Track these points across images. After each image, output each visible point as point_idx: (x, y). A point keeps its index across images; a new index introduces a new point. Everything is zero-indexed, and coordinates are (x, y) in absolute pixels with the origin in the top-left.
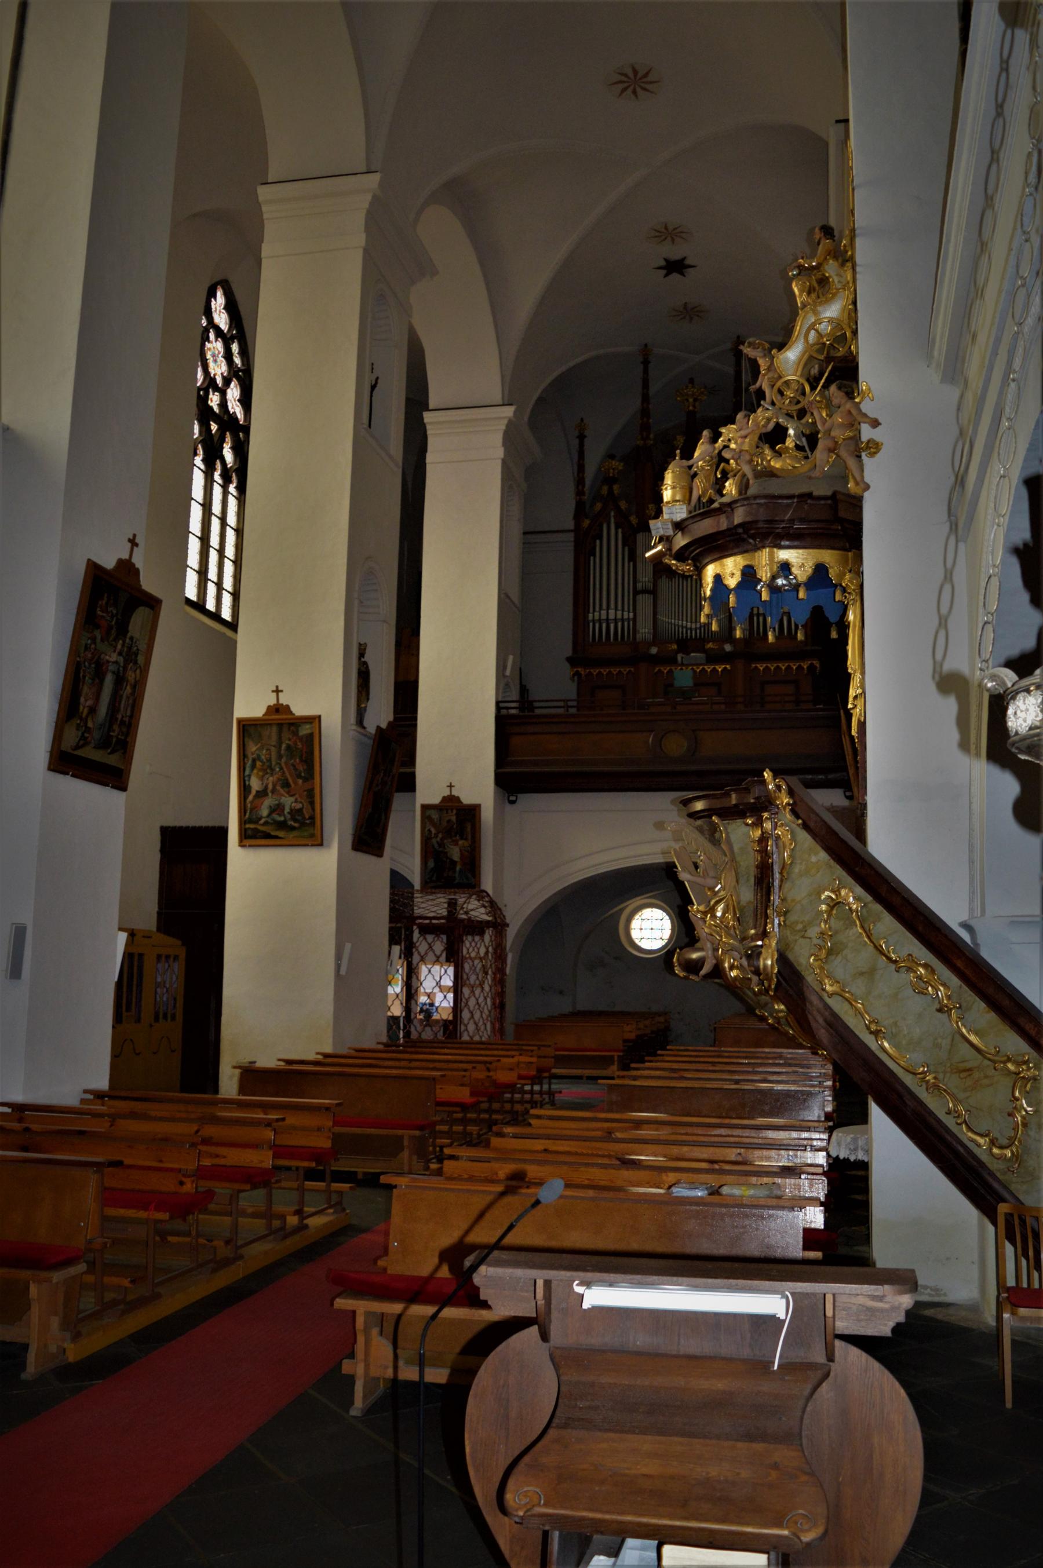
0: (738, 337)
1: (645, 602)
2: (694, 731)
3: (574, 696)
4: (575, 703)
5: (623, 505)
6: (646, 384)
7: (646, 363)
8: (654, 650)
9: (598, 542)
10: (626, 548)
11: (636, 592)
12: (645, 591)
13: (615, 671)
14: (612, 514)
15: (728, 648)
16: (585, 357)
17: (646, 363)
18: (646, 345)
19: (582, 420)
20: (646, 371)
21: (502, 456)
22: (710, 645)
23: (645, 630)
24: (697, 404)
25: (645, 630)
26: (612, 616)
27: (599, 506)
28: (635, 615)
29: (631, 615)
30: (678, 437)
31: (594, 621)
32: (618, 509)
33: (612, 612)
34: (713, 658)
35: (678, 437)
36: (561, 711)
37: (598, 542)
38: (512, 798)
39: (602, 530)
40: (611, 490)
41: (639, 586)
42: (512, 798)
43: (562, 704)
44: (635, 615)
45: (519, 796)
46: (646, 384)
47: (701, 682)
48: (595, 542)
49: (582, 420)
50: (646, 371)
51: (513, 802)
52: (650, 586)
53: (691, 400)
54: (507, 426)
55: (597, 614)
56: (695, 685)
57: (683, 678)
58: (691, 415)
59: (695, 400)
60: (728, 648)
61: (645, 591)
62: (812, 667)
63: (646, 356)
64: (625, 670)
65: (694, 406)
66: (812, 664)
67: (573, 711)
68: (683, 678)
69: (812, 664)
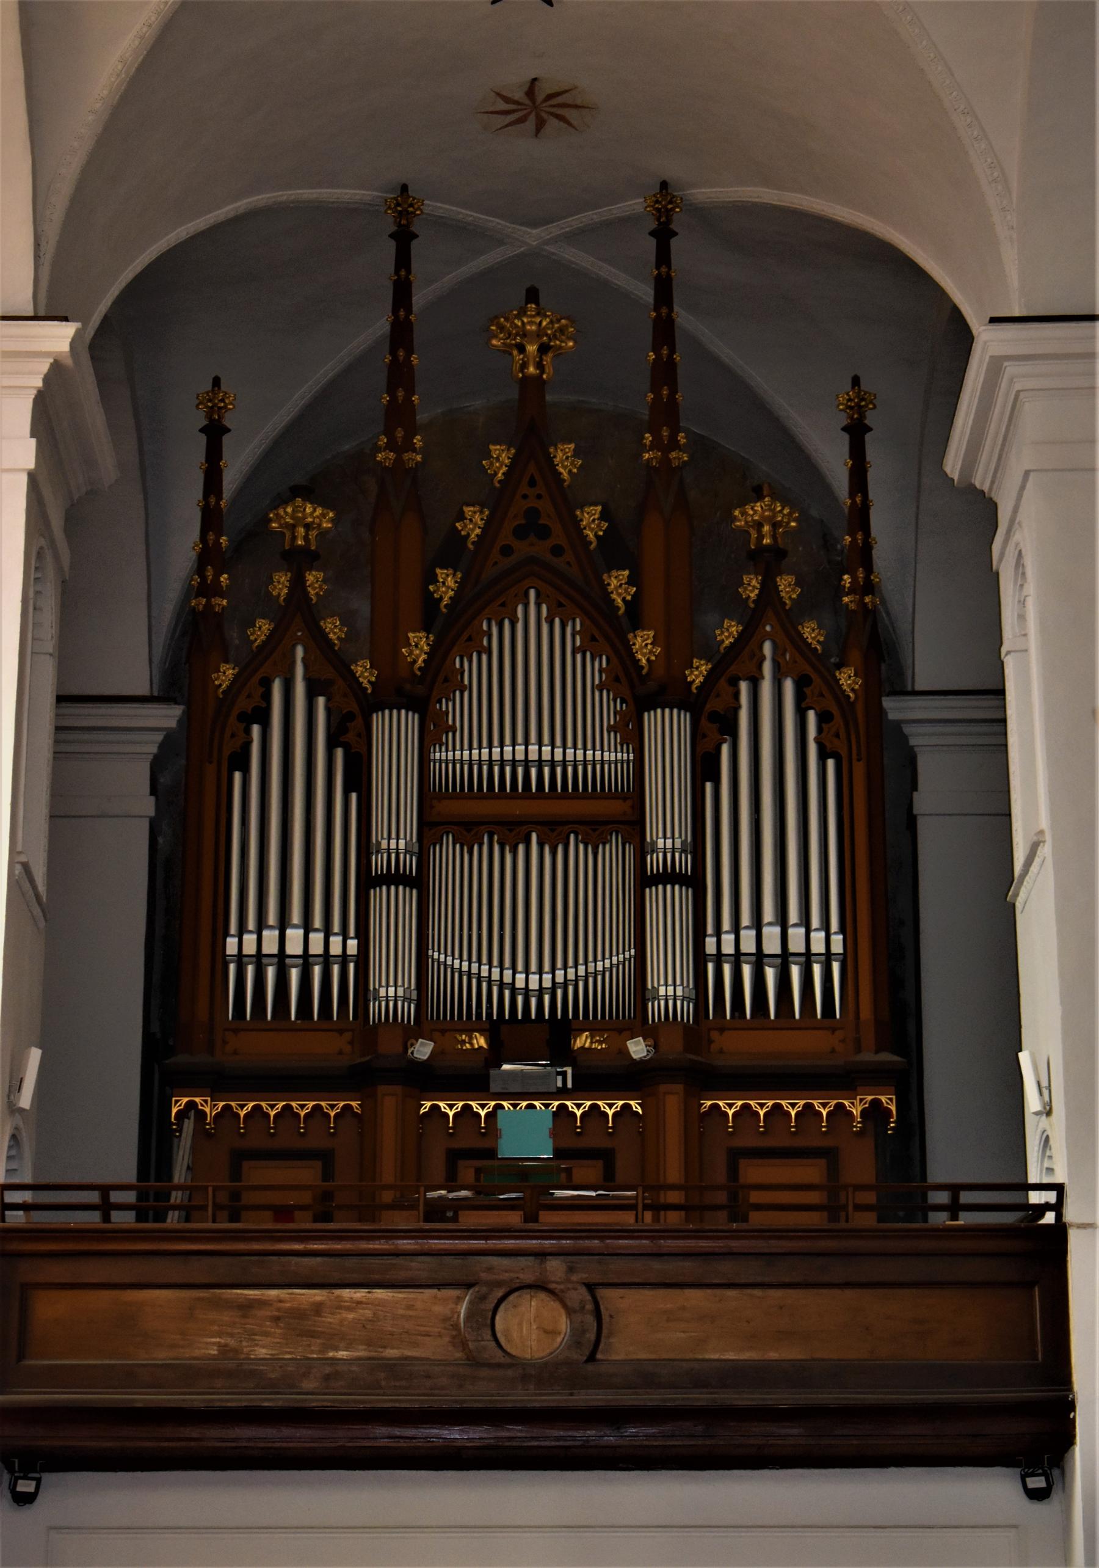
0: (664, 185)
1: (393, 907)
2: (591, 1287)
3: (130, 1174)
4: (130, 1197)
5: (333, 629)
6: (402, 292)
7: (403, 238)
8: (423, 1050)
9: (256, 729)
10: (339, 753)
11: (368, 881)
12: (394, 878)
13: (303, 1107)
14: (300, 652)
15: (638, 1048)
16: (242, 205)
17: (403, 238)
18: (404, 188)
19: (216, 382)
20: (403, 260)
21: (31, 464)
22: (582, 1041)
23: (392, 990)
24: (547, 359)
25: (392, 990)
26: (294, 947)
27: (262, 629)
28: (364, 947)
29: (353, 945)
30: (496, 450)
31: (240, 956)
32: (318, 640)
33: (295, 935)
34: (593, 1080)
35: (496, 450)
36: (93, 1218)
37: (256, 729)
38: (25, 1486)
39: (267, 697)
40: (298, 584)
41: (378, 863)
42: (25, 1486)
43: (94, 1197)
44: (364, 947)
45: (47, 1478)
46: (402, 292)
47: (574, 1146)
48: (248, 731)
49: (216, 382)
50: (403, 260)
51: (24, 1500)
52: (684, 863)
53: (532, 348)
54: (47, 379)
55: (250, 939)
56: (560, 1153)
57: (526, 1131)
58: (532, 387)
59: (543, 349)
60: (638, 1048)
61: (394, 878)
62: (875, 1111)
63: (404, 222)
64: (333, 1107)
65: (540, 366)
66: (876, 1103)
67: (124, 1219)
68: (526, 1131)
69: (876, 1103)
